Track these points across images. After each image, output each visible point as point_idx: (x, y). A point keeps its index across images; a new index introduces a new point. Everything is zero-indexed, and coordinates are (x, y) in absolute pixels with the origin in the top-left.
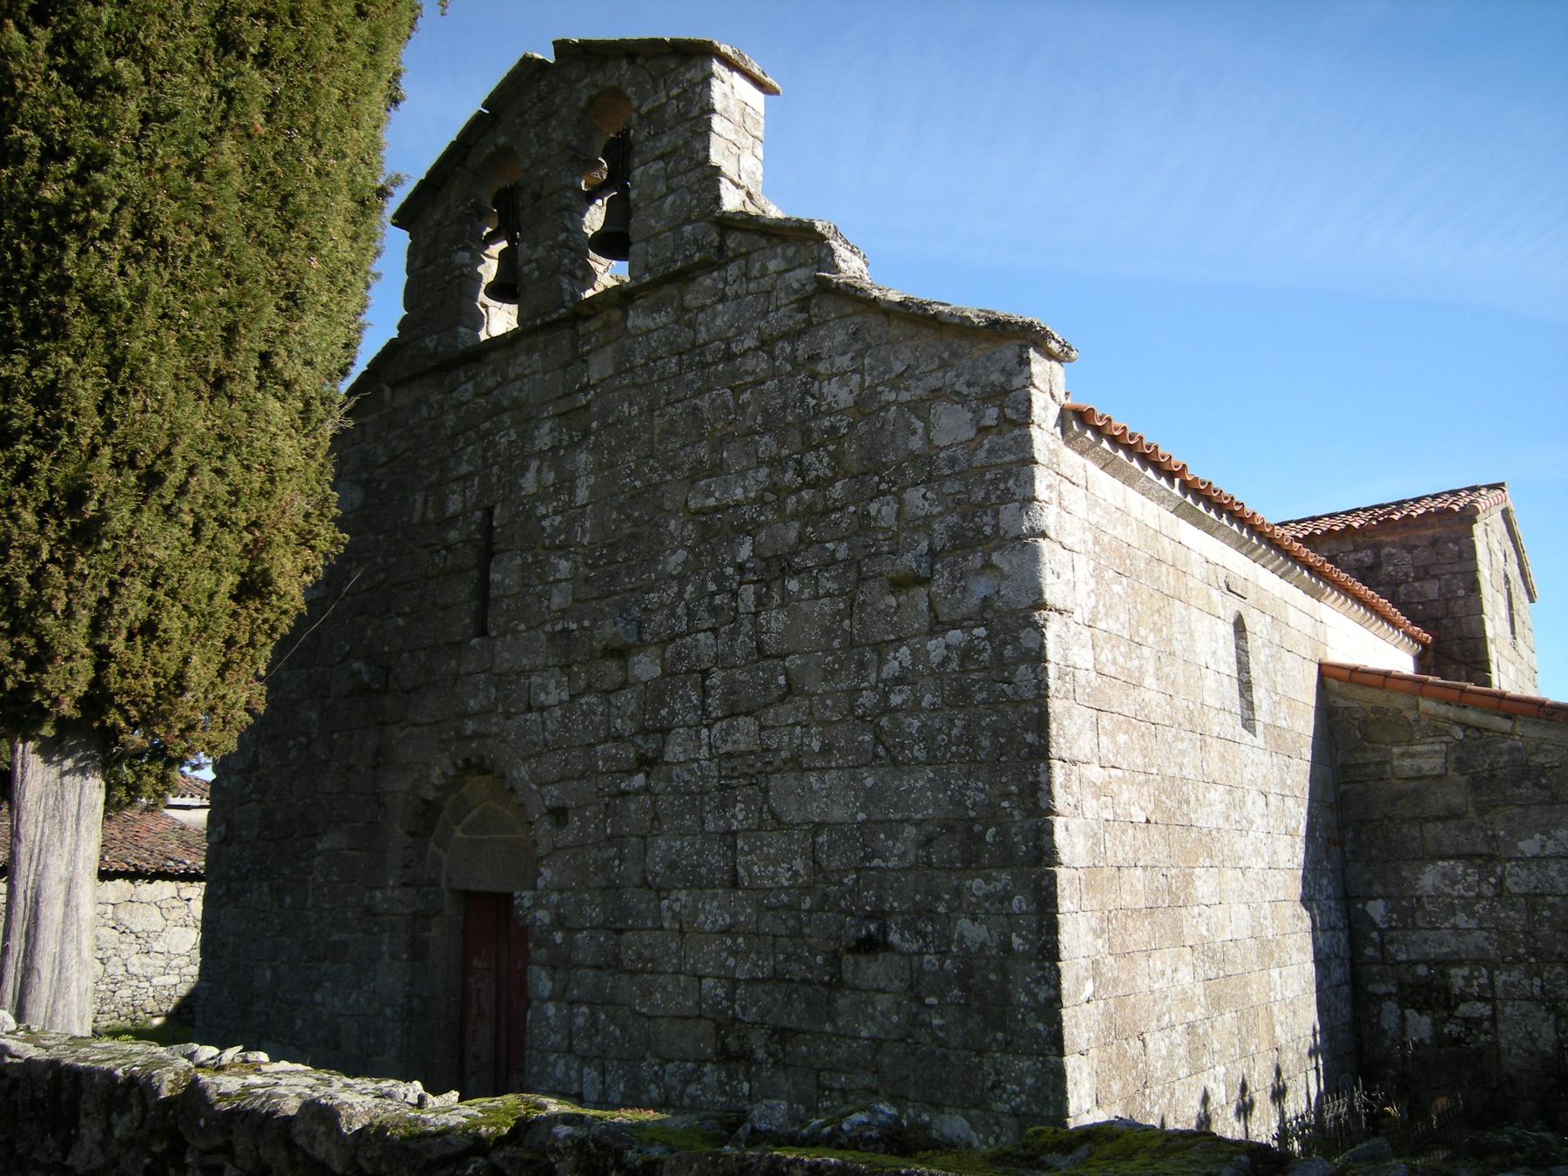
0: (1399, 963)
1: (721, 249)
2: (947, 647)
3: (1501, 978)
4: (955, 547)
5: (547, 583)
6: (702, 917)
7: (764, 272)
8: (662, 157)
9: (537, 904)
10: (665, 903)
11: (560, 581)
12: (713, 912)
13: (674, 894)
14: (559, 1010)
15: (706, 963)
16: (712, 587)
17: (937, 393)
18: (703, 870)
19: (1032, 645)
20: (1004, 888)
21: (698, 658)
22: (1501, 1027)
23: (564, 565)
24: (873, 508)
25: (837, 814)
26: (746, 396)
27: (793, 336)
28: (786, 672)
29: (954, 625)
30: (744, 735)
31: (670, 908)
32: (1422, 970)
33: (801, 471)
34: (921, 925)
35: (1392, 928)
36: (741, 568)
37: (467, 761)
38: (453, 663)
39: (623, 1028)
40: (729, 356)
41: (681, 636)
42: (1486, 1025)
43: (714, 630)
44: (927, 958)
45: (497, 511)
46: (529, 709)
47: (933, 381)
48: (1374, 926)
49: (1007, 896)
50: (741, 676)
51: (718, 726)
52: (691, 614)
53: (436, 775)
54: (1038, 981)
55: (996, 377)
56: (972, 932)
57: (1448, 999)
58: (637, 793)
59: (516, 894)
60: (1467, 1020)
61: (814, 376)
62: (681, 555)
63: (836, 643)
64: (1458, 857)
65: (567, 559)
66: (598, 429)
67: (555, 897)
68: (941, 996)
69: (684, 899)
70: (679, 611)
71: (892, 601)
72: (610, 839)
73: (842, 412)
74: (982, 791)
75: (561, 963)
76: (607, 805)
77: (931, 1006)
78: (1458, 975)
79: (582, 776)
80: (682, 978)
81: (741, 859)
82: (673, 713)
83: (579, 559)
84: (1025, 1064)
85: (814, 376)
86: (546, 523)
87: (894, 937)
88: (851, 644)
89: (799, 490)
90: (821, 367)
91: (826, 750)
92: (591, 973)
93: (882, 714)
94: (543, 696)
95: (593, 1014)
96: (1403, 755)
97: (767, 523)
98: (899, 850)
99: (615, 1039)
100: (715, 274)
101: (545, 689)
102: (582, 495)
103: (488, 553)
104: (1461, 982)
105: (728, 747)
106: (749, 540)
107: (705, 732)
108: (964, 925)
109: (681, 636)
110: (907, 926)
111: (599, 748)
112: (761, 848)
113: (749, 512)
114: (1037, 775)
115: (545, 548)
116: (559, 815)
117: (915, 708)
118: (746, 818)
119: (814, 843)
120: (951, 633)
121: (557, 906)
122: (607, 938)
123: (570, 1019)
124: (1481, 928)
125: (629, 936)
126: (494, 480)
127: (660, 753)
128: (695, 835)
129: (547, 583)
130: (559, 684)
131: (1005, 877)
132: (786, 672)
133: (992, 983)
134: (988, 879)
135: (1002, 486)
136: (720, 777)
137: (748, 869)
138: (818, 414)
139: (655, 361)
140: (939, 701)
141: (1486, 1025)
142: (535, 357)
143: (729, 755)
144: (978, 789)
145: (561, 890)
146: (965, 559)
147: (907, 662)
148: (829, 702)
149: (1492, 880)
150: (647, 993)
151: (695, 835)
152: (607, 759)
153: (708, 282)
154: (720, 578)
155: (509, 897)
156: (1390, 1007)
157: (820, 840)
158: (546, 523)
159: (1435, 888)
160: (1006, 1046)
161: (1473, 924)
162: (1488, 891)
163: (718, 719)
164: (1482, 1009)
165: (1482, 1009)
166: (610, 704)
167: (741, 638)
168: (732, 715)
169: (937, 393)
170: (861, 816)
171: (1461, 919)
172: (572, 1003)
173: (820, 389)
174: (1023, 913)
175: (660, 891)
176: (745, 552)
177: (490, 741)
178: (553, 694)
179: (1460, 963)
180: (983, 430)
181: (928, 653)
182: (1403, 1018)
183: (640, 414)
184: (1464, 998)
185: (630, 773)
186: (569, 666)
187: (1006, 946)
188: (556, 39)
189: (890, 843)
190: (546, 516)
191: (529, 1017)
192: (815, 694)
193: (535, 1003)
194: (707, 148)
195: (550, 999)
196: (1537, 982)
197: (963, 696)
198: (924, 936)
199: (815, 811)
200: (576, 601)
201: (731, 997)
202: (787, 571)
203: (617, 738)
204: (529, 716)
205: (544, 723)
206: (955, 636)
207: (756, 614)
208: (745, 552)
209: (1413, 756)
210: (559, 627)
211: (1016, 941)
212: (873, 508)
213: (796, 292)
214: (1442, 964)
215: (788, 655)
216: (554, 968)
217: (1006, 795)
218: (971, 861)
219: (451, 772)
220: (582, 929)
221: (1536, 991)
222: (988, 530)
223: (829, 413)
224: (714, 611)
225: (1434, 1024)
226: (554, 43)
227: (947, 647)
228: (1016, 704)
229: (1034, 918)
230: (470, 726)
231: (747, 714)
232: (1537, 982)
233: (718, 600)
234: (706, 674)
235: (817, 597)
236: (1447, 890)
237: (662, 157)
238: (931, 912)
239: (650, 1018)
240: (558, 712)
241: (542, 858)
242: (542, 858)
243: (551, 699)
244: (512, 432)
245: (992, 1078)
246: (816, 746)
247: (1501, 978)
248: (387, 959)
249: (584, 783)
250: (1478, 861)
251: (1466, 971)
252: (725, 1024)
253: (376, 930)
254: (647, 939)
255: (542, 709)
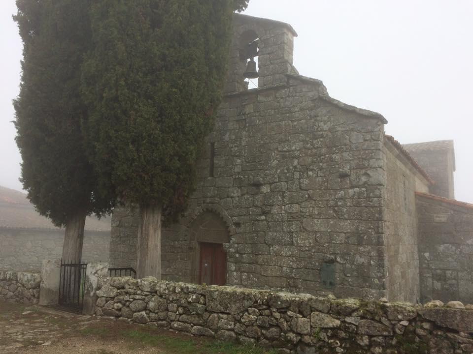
0: (432, 269)
1: (288, 82)
2: (355, 192)
3: (460, 274)
4: (357, 168)
5: (233, 165)
6: (282, 252)
7: (301, 91)
8: (269, 54)
9: (230, 247)
10: (271, 248)
11: (237, 165)
12: (285, 251)
13: (274, 246)
14: (237, 274)
15: (284, 264)
16: (286, 171)
17: (352, 130)
18: (283, 241)
19: (378, 194)
20: (369, 250)
21: (282, 188)
22: (459, 287)
23: (239, 161)
24: (334, 156)
25: (323, 229)
26: (295, 123)
27: (311, 109)
28: (308, 194)
29: (356, 187)
30: (296, 208)
31: (273, 250)
32: (438, 271)
33: (312, 144)
34: (346, 257)
35: (431, 260)
36: (295, 167)
37: (207, 209)
38: (202, 183)
39: (258, 279)
40: (290, 112)
41: (276, 183)
42: (455, 286)
43: (287, 182)
44: (347, 265)
45: (216, 144)
46: (228, 197)
47: (351, 127)
48: (426, 259)
49: (369, 252)
50: (294, 194)
51: (287, 206)
52: (279, 177)
53: (197, 212)
54: (378, 272)
55: (369, 128)
56: (361, 260)
57: (445, 279)
58: (263, 221)
59: (224, 244)
60: (450, 284)
61: (316, 120)
62: (276, 162)
63: (323, 188)
64: (450, 243)
65: (240, 159)
66: (249, 126)
67: (236, 245)
68: (352, 274)
69: (277, 248)
70: (276, 176)
71: (339, 180)
72: (253, 231)
73: (325, 131)
74: (364, 227)
75: (237, 262)
76: (253, 223)
77: (348, 276)
78: (449, 273)
79: (245, 215)
80: (277, 267)
81: (294, 239)
82: (273, 202)
83: (244, 160)
84: (374, 291)
85: (316, 120)
86: (233, 149)
87: (338, 259)
88: (327, 189)
89: (311, 149)
90: (318, 118)
91: (319, 214)
92: (248, 265)
93: (336, 206)
94: (232, 194)
95: (248, 275)
96: (437, 217)
97: (303, 157)
98: (340, 238)
99: (256, 281)
100: (286, 89)
101: (233, 193)
102: (243, 143)
103: (213, 154)
104: (449, 275)
105: (291, 211)
106: (297, 160)
107: (283, 207)
108: (358, 257)
109: (276, 183)
110: (342, 257)
111: (251, 209)
112: (300, 236)
113: (297, 153)
114: (378, 224)
115: (232, 156)
116: (238, 225)
117: (345, 205)
118: (296, 229)
119: (316, 236)
120: (355, 189)
121: (237, 248)
122: (253, 256)
123: (241, 277)
124: (455, 262)
125: (259, 256)
126: (214, 136)
127: (270, 211)
128: (280, 232)
129: (233, 165)
130: (237, 191)
131: (369, 247)
132: (308, 194)
133: (365, 272)
134: (364, 248)
135: (371, 155)
136: (288, 218)
137: (297, 242)
138: (318, 131)
139: (267, 110)
140: (352, 205)
141: (455, 286)
142: (227, 104)
143: (291, 213)
144: (362, 226)
145: (238, 244)
146: (360, 172)
147: (343, 195)
148: (320, 203)
149: (459, 250)
150: (265, 271)
151: (280, 232)
152: (253, 212)
153: (284, 91)
154: (288, 169)
155: (221, 245)
156: (430, 279)
157: (318, 235)
158: (233, 149)
159: (443, 250)
160: (370, 287)
161: (453, 260)
162: (458, 253)
163: (287, 204)
164: (454, 281)
165: (454, 281)
166: (254, 198)
167: (295, 185)
168: (292, 203)
169: (352, 130)
170: (329, 230)
171: (450, 259)
172: (241, 272)
173: (318, 124)
174: (374, 256)
175: (269, 246)
176: (296, 163)
177: (215, 205)
178: (236, 193)
179: (449, 270)
180: (365, 140)
181: (349, 193)
182: (433, 282)
183: (262, 124)
184: (449, 279)
185: (260, 215)
186: (241, 187)
187: (370, 264)
188: (454, 142)
189: (337, 237)
190: (232, 147)
191: (228, 275)
192: (316, 200)
193: (229, 272)
194: (283, 54)
195: (234, 271)
196: (470, 276)
197: (358, 205)
198: (347, 260)
199: (316, 228)
200: (242, 170)
201: (291, 272)
202: (308, 169)
203: (256, 207)
204: (228, 199)
205: (233, 201)
206: (357, 190)
207: (299, 179)
208: (296, 163)
209: (439, 217)
210: (237, 177)
211: (372, 262)
212: (334, 156)
213: (311, 98)
214: (444, 270)
215: (309, 190)
216: (236, 263)
217: (370, 228)
218: (360, 243)
219: (201, 211)
220: (245, 254)
221: (470, 278)
222: (366, 165)
223: (321, 131)
224: (287, 178)
225: (442, 285)
226: (452, 141)
227: (355, 192)
228: (373, 207)
229: (377, 257)
230: (208, 200)
231: (297, 203)
232: (470, 276)
233: (288, 175)
234: (284, 193)
235: (317, 176)
236: (447, 252)
237: (269, 54)
238: (348, 254)
239: (266, 277)
240: (237, 199)
241: (231, 236)
242: (231, 236)
243: (236, 195)
244: (220, 123)
245: (365, 294)
246: (316, 213)
247: (460, 274)
248: (180, 260)
249: (246, 217)
250: (456, 245)
251: (450, 272)
252: (289, 278)
253: (176, 252)
254: (266, 257)
255: (232, 197)
